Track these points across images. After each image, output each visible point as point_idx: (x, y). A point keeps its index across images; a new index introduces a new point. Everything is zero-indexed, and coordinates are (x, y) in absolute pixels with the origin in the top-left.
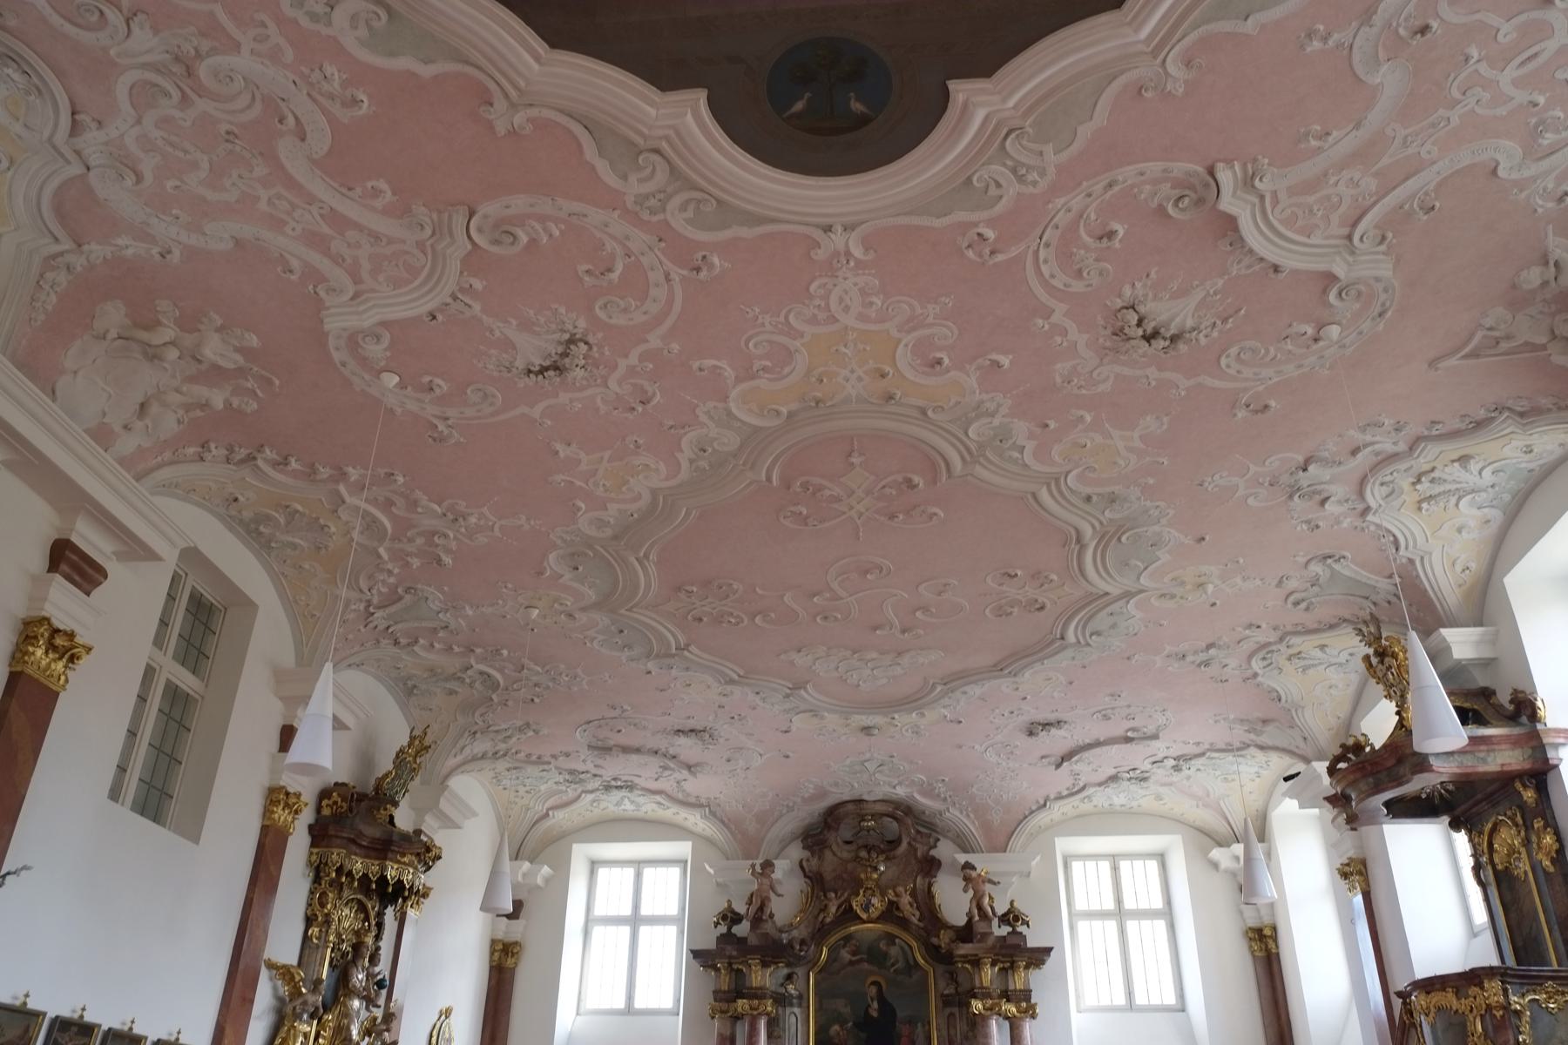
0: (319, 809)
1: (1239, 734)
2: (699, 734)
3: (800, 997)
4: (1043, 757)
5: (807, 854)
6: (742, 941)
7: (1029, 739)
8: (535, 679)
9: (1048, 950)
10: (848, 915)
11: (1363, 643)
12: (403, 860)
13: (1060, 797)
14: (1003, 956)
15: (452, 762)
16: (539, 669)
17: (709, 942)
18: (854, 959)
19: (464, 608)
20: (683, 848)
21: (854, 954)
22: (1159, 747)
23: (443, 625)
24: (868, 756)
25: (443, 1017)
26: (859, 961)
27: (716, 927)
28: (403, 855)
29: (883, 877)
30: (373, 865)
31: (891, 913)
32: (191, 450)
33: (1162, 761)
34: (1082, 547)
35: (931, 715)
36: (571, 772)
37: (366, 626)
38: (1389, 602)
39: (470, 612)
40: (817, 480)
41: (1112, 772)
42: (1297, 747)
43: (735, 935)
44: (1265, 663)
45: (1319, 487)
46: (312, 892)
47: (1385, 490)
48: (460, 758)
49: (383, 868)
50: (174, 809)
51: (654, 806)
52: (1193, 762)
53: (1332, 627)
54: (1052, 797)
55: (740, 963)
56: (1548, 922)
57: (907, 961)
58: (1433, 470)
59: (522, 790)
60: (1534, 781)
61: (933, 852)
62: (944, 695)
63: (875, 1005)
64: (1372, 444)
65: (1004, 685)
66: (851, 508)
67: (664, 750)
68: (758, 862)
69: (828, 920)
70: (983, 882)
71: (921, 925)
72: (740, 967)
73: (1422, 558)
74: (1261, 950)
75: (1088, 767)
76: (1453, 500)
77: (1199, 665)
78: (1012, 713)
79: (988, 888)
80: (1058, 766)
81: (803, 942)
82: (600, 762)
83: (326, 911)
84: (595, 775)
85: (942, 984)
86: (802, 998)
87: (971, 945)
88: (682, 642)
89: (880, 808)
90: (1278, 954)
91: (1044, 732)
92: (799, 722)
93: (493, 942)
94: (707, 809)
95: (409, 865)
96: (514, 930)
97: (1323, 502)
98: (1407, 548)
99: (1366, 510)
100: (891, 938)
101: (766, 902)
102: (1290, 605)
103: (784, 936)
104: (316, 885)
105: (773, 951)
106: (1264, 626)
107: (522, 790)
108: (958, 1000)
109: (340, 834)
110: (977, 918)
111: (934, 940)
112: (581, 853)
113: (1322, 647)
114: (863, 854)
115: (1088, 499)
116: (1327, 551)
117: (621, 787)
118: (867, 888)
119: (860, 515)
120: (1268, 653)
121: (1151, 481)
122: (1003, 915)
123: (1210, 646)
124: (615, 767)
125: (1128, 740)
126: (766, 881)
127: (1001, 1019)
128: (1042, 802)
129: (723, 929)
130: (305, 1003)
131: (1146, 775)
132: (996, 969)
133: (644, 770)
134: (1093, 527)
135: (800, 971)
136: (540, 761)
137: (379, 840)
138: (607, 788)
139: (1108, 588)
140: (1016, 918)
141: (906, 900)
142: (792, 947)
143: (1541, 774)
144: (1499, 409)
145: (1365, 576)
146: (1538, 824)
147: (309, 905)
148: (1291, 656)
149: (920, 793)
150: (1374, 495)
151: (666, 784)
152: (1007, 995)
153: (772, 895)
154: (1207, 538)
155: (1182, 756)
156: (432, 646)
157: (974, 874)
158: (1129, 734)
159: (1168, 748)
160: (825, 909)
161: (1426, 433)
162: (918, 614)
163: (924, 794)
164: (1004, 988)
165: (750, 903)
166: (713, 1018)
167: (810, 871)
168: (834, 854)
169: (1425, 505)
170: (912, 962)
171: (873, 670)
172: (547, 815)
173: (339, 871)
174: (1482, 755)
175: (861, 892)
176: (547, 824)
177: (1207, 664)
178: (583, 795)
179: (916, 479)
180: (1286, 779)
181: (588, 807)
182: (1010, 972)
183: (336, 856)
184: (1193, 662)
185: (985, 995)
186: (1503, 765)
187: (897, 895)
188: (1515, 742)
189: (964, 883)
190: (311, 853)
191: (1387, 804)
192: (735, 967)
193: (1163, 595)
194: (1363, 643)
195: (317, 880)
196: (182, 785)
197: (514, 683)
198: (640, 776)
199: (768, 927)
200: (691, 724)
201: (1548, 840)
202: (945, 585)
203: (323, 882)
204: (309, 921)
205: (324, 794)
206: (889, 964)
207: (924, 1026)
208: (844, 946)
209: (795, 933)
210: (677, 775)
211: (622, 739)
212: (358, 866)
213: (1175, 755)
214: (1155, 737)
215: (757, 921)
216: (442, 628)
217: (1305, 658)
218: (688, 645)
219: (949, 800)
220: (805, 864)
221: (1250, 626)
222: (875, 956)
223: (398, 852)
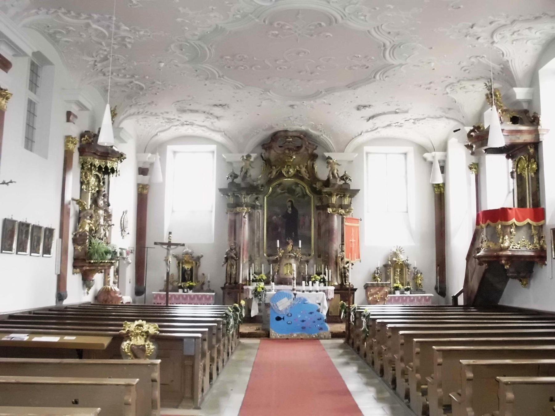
0: (81, 141)
1: (439, 113)
2: (223, 107)
3: (261, 206)
4: (362, 117)
5: (264, 151)
6: (238, 185)
7: (358, 111)
8: (158, 86)
9: (358, 191)
10: (280, 175)
11: (487, 89)
12: (113, 160)
13: (367, 132)
14: (341, 192)
15: (122, 117)
16: (160, 83)
17: (225, 186)
18: (282, 192)
19: (134, 63)
20: (214, 147)
21: (282, 190)
22: (408, 116)
23: (124, 68)
24: (291, 115)
25: (125, 214)
26: (284, 193)
27: (227, 179)
28: (113, 158)
29: (294, 161)
30: (102, 162)
31: (298, 175)
32: (34, 11)
33: (408, 120)
34: (385, 50)
35: (319, 101)
36: (168, 119)
37: (94, 69)
38: (499, 74)
39: (135, 64)
40: (282, 23)
41: (389, 123)
42: (460, 119)
43: (235, 183)
44: (451, 89)
45: (477, 34)
46: (81, 173)
47: (500, 36)
48: (125, 115)
49: (106, 163)
50: (36, 146)
51: (202, 132)
52: (421, 121)
53: (478, 79)
54: (364, 131)
55: (238, 194)
56: (529, 193)
57: (303, 193)
58: (519, 31)
59: (147, 125)
60: (534, 146)
61: (315, 152)
62: (325, 95)
63: (290, 209)
64: (498, 21)
65: (350, 92)
66: (296, 32)
67: (207, 111)
68: (245, 154)
69: (272, 177)
70: (335, 164)
71: (309, 179)
72: (238, 195)
73: (511, 61)
74: (438, 192)
75: (378, 121)
76: (525, 41)
77: (426, 89)
78: (351, 102)
79: (336, 167)
80: (368, 120)
81: (262, 186)
82: (180, 115)
83: (88, 179)
84: (178, 120)
85: (316, 201)
86: (262, 206)
87: (328, 188)
88: (221, 74)
89: (295, 134)
90: (444, 193)
91: (363, 109)
92: (264, 103)
93: (138, 185)
94: (223, 133)
95: (115, 161)
96: (144, 179)
97: (478, 38)
98: (507, 56)
99: (493, 43)
100: (297, 184)
101: (248, 171)
102: (462, 71)
103: (255, 183)
104: (83, 170)
105: (252, 189)
106: (452, 77)
107: (147, 125)
108: (323, 207)
109: (90, 151)
110: (332, 178)
111: (314, 186)
112: (170, 148)
113: (473, 85)
114: (287, 151)
115: (389, 33)
116: (478, 55)
117: (188, 124)
118: (288, 165)
119: (299, 34)
120: (453, 86)
121: (414, 29)
122: (342, 177)
123: (431, 83)
124: (186, 117)
125: (396, 113)
126: (248, 162)
127: (338, 215)
128: (360, 133)
129: (230, 180)
130: (87, 213)
131: (402, 125)
132: (338, 197)
133: (199, 119)
134: (390, 42)
135: (261, 196)
136: (156, 115)
137: (103, 152)
138: (183, 125)
139: (394, 63)
140: (347, 178)
141: (303, 170)
142: (258, 187)
143: (536, 145)
144: (545, 14)
145: (492, 64)
146: (533, 160)
147: (81, 177)
148: (461, 87)
149: (311, 129)
150: (496, 38)
151: (207, 123)
152: (341, 206)
153: (250, 168)
154: (433, 48)
155: (417, 119)
156: (118, 75)
157: (331, 161)
158: (397, 111)
159: (411, 116)
160: (271, 173)
161: (517, 19)
162: (318, 68)
163: (312, 129)
164: (340, 204)
165: (241, 171)
166: (227, 213)
167: (265, 158)
168: (275, 151)
169: (514, 42)
170: (305, 194)
171: (297, 86)
172: (157, 135)
173: (91, 165)
174: (518, 136)
175: (286, 166)
176: (156, 138)
177: (429, 89)
178: (172, 127)
179: (323, 24)
180: (455, 131)
181: (173, 132)
182: (343, 198)
183: (89, 159)
184: (424, 88)
185: (333, 206)
186: (525, 140)
187: (300, 167)
188: (530, 132)
189: (327, 164)
190: (80, 159)
191: (486, 150)
192: (236, 195)
193: (414, 66)
194: (487, 89)
195: (83, 168)
196: (37, 137)
197: (149, 88)
198: (196, 120)
199: (248, 180)
200: (221, 103)
201: (534, 166)
202: (330, 59)
203: (85, 169)
204: (82, 183)
205: (82, 136)
206: (296, 193)
207: (308, 217)
208: (278, 187)
209: (259, 182)
210: (212, 120)
211: (191, 107)
212: (97, 162)
213: (414, 118)
214: (406, 112)
215: (244, 177)
216: (123, 69)
217: (466, 89)
218: (223, 76)
219: (323, 131)
220: (263, 155)
221: (447, 77)
222: (290, 191)
223: (111, 157)
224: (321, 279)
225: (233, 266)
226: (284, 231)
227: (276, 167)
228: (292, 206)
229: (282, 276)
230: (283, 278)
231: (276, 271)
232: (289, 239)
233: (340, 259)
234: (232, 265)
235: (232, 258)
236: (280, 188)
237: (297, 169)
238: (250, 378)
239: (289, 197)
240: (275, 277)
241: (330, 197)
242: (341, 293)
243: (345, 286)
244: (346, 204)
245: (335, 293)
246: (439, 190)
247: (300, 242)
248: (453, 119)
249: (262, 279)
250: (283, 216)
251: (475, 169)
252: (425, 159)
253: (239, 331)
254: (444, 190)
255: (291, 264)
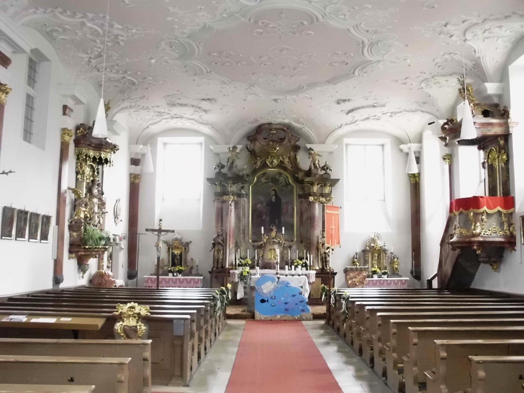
0: (76, 133)
1: (414, 107)
2: (211, 101)
3: (246, 195)
4: (342, 111)
5: (249, 143)
6: (225, 175)
7: (338, 105)
8: (149, 82)
9: (338, 180)
10: (264, 165)
11: (459, 84)
12: (107, 151)
13: (347, 124)
14: (322, 182)
15: (115, 111)
16: (151, 79)
17: (212, 175)
18: (267, 181)
19: (126, 59)
20: (202, 139)
21: (266, 179)
22: (385, 109)
23: (117, 64)
24: (275, 109)
25: (118, 202)
26: (268, 182)
27: (215, 169)
28: (107, 149)
29: (278, 152)
30: (97, 153)
31: (281, 165)
32: (32, 10)
33: (386, 114)
34: (363, 47)
35: (301, 96)
36: (159, 112)
37: (88, 66)
38: (471, 69)
39: (128, 60)
40: (266, 21)
41: (367, 116)
42: (435, 113)
43: (222, 172)
44: (426, 84)
45: (450, 32)
46: (77, 163)
47: (473, 34)
48: (118, 109)
49: (100, 154)
50: (34, 138)
51: (190, 124)
52: (397, 114)
53: (451, 75)
54: (344, 124)
55: (225, 183)
56: (499, 182)
57: (286, 182)
58: (490, 29)
59: (139, 118)
60: (504, 138)
61: (297, 143)
62: (307, 90)
63: (274, 197)
64: (470, 20)
65: (330, 87)
66: (279, 30)
67: (196, 105)
68: (231, 146)
69: (257, 167)
70: (316, 155)
71: (292, 169)
72: (225, 184)
73: (483, 57)
74: (414, 181)
75: (357, 115)
76: (496, 39)
77: (403, 84)
78: (332, 96)
79: (317, 157)
80: (348, 114)
81: (248, 176)
82: (170, 109)
83: (83, 169)
84: (168, 113)
85: (299, 190)
86: (247, 195)
87: (310, 178)
88: (209, 70)
89: (278, 127)
90: (419, 183)
91: (343, 103)
92: (249, 97)
93: (131, 174)
94: (211, 126)
95: (108, 152)
96: (136, 169)
97: (451, 36)
98: (478, 52)
99: (465, 40)
100: (280, 174)
101: (234, 161)
102: (436, 67)
103: (240, 173)
104: (78, 161)
105: (238, 179)
106: (427, 73)
107: (139, 118)
108: (305, 196)
109: (85, 143)
110: (313, 168)
111: (297, 175)
112: (161, 140)
113: (447, 81)
114: (271, 143)
115: (368, 31)
116: (452, 52)
117: (178, 117)
118: (272, 156)
119: (283, 33)
120: (427, 81)
121: (390, 27)
122: (323, 167)
123: (407, 78)
124: (175, 111)
125: (374, 106)
126: (234, 153)
127: (319, 203)
128: (340, 126)
129: (217, 170)
130: (82, 201)
131: (379, 118)
132: (319, 186)
133: (188, 112)
134: (369, 40)
135: (246, 185)
136: (147, 108)
137: (98, 144)
138: (172, 118)
139: (372, 59)
140: (327, 168)
141: (286, 160)
142: (244, 177)
143: (507, 137)
144: (514, 13)
145: (464, 61)
146: (503, 151)
147: (77, 168)
148: (436, 83)
149: (294, 122)
150: (468, 36)
151: (195, 117)
152: (322, 195)
153: (236, 158)
154: (409, 45)
155: (393, 112)
156: (111, 71)
157: (313, 152)
158: (375, 105)
159: (388, 109)
160: (256, 163)
161: (488, 18)
162: (300, 64)
163: (295, 122)
164: (321, 193)
165: (228, 162)
166: (214, 202)
167: (250, 149)
168: (260, 143)
169: (486, 40)
170: (288, 183)
171: (281, 81)
172: (148, 127)
173: (86, 156)
174: (489, 129)
175: (270, 157)
176: (147, 130)
177: (405, 84)
178: (163, 120)
179: (305, 22)
180: (429, 124)
181: (164, 125)
182: (324, 187)
183: (84, 151)
184: (400, 83)
185: (314, 195)
186: (495, 132)
187: (283, 158)
188: (500, 125)
189: (309, 155)
190: (75, 150)
191: (458, 142)
192: (223, 184)
193: (391, 62)
194: (459, 84)
195: (78, 159)
196: (35, 130)
197: (141, 83)
198: (185, 114)
199: (234, 170)
200: (208, 97)
201: (504, 157)
202: (311, 56)
203: (80, 159)
204: (77, 173)
205: (78, 128)
206: (280, 183)
207: (291, 205)
208: (263, 177)
209: (245, 172)
210: (200, 114)
211: (181, 102)
212: (92, 153)
213: (391, 112)
214: (384, 106)
215: (231, 167)
216: (116, 65)
217: (440, 84)
218: (210, 72)
219: (305, 124)
220: (248, 147)
221: (422, 73)
222: (274, 180)
223: (104, 148)
224: (303, 263)
225: (220, 251)
226: (268, 218)
227: (260, 158)
228: (276, 195)
229: (266, 261)
230: (267, 263)
231: (261, 256)
232: (273, 226)
233: (321, 245)
234: (219, 251)
235: (219, 243)
236: (264, 178)
237: (281, 159)
238: (236, 357)
239: (273, 186)
240: (259, 261)
241: (312, 186)
242: (322, 276)
243: (326, 270)
244: (326, 192)
245: (316, 277)
246: (415, 180)
247: (283, 228)
248: (427, 112)
249: (247, 263)
250: (267, 204)
251: (449, 159)
252: (401, 151)
253: (225, 312)
254: (419, 180)
255: (274, 250)
